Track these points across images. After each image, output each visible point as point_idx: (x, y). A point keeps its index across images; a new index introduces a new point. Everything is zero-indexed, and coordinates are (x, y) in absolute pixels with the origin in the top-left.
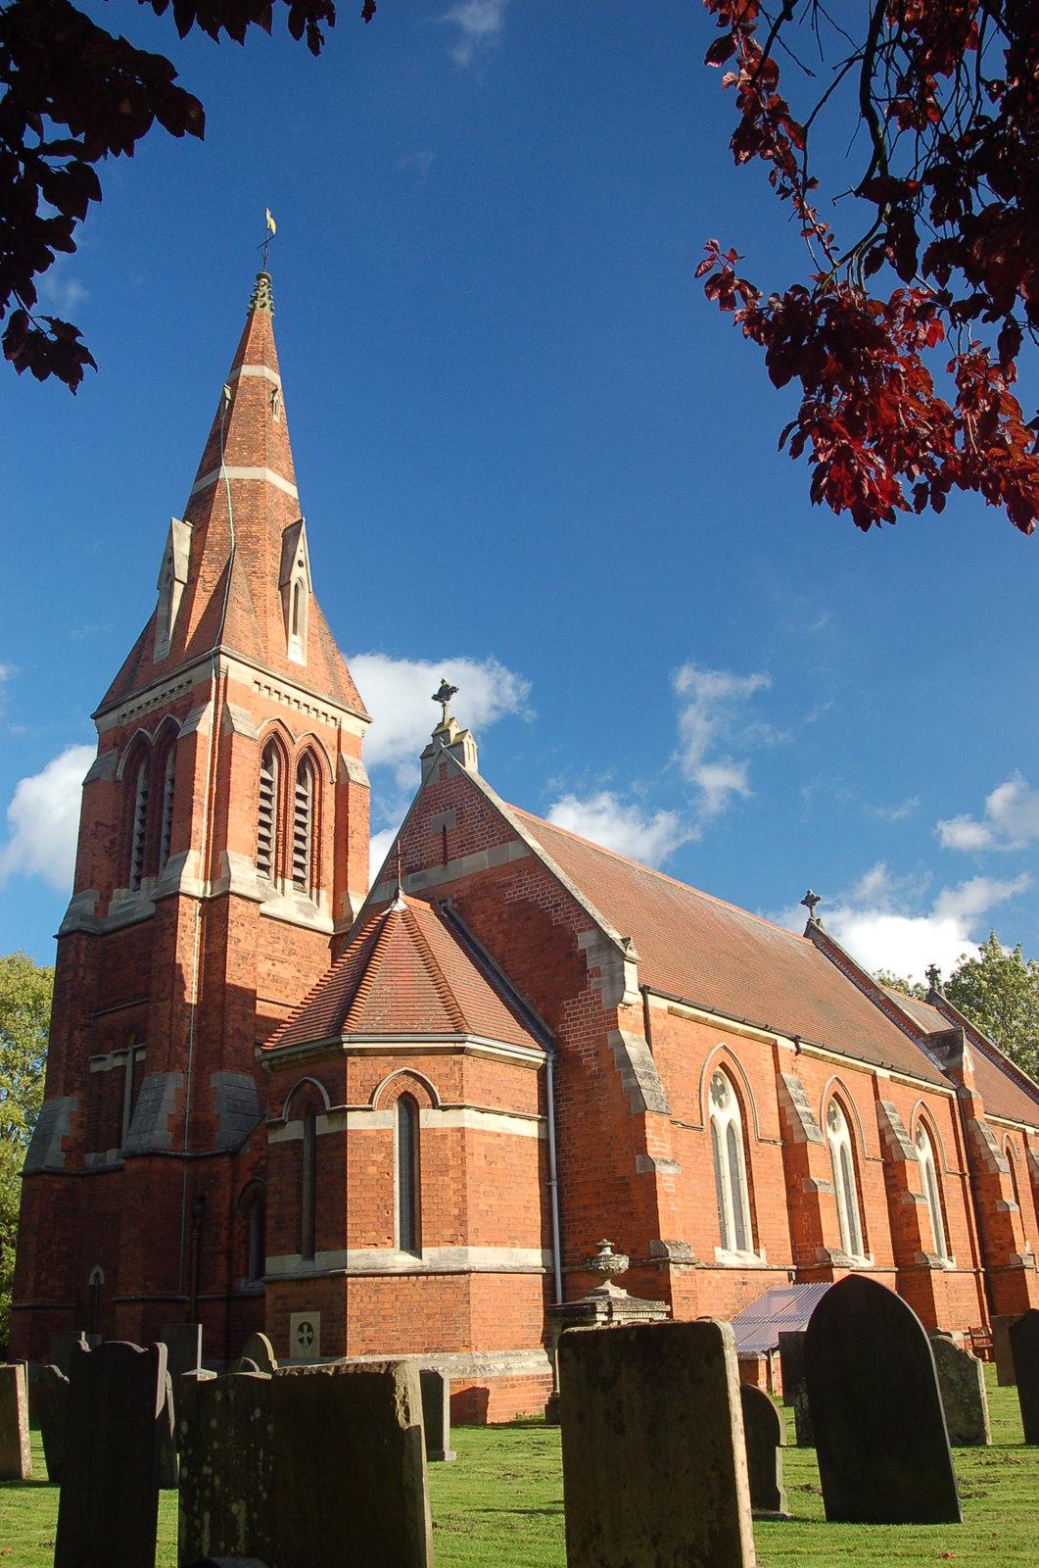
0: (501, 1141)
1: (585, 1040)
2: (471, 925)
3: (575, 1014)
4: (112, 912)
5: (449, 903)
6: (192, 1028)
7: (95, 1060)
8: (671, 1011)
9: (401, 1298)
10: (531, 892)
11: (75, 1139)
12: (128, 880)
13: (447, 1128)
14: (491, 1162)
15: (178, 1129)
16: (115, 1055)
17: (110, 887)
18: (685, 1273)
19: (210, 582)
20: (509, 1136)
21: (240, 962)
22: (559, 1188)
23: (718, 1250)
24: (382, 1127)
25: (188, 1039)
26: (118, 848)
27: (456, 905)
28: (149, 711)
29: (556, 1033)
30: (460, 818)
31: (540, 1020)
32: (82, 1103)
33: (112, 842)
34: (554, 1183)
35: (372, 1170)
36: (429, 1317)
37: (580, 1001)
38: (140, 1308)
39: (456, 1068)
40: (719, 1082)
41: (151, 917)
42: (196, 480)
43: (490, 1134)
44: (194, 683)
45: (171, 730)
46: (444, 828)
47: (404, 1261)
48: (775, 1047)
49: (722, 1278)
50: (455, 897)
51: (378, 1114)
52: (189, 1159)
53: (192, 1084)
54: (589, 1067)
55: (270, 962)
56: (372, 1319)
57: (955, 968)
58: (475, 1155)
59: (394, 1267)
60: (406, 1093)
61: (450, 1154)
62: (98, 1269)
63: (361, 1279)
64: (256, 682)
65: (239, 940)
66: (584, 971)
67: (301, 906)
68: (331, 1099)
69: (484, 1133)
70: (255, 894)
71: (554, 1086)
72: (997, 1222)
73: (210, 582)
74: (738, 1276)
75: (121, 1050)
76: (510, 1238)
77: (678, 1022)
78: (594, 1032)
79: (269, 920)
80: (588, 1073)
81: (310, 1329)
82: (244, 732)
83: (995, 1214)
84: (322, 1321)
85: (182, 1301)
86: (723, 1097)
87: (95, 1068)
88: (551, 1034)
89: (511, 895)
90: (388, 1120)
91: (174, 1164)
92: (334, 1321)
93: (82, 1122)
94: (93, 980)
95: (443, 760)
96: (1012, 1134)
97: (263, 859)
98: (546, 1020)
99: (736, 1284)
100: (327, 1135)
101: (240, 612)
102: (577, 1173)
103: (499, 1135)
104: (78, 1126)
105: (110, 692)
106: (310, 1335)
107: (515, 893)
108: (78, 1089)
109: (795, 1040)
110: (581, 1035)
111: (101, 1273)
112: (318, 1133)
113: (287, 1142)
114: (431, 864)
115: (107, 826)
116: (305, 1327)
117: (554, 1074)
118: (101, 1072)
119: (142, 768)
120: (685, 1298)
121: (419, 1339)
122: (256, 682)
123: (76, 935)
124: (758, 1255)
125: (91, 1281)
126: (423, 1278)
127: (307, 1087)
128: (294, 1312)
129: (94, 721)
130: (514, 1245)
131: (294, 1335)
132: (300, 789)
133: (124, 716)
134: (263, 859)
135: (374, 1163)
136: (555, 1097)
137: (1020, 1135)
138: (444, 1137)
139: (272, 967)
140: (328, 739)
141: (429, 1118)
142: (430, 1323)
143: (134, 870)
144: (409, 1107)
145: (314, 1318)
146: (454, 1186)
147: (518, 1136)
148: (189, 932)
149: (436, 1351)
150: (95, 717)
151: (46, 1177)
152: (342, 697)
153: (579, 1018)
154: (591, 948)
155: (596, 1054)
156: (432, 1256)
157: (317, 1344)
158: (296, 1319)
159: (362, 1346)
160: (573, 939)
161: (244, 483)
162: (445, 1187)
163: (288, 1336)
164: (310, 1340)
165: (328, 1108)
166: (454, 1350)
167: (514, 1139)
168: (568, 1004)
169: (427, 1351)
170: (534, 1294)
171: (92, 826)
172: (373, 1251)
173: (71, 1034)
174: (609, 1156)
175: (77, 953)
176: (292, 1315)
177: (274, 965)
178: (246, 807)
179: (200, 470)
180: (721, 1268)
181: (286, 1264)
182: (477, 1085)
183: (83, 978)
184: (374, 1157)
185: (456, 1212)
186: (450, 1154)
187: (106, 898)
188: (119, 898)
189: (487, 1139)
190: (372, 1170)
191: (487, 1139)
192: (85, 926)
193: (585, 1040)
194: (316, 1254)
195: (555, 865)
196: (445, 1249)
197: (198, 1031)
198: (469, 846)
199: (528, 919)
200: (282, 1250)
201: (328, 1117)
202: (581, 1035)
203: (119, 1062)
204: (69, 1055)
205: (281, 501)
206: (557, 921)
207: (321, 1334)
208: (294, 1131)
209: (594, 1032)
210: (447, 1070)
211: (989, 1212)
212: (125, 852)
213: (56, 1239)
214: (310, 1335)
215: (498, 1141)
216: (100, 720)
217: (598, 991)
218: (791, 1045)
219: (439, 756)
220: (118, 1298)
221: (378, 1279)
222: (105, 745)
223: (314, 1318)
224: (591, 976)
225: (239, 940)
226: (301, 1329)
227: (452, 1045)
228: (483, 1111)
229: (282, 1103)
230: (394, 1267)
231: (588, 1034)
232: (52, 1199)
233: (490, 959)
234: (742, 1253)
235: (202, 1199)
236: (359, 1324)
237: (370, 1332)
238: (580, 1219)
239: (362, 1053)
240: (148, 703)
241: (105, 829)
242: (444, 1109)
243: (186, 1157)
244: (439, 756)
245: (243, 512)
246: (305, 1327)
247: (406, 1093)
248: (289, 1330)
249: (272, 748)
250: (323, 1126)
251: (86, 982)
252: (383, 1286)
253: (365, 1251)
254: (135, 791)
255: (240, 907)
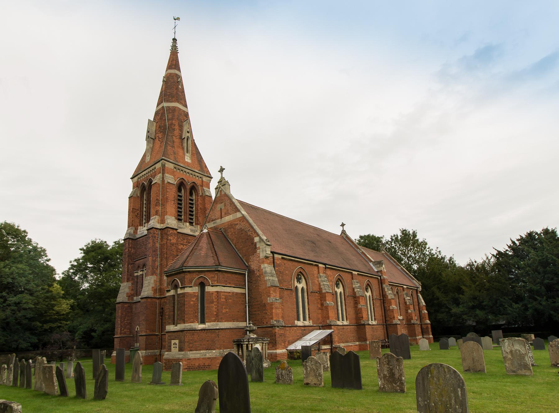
0: (230, 294)
1: (256, 267)
2: (228, 235)
3: (253, 259)
4: (138, 233)
5: (222, 229)
6: (158, 264)
7: (135, 272)
8: (282, 258)
9: (200, 336)
10: (243, 226)
11: (131, 293)
12: (142, 224)
13: (213, 291)
14: (227, 300)
15: (155, 291)
16: (140, 271)
17: (138, 226)
18: (281, 329)
19: (161, 138)
20: (233, 293)
21: (171, 246)
22: (248, 306)
23: (296, 322)
24: (195, 291)
25: (157, 266)
26: (139, 215)
27: (224, 230)
28: (145, 176)
29: (249, 265)
30: (225, 206)
31: (245, 261)
32: (132, 284)
33: (138, 214)
34: (247, 305)
35: (192, 303)
36: (208, 341)
37: (255, 256)
38: (145, 337)
39: (216, 275)
40: (299, 277)
41: (146, 235)
42: (157, 107)
43: (226, 292)
44: (156, 168)
45: (151, 181)
46: (221, 208)
47: (201, 326)
48: (317, 266)
49: (297, 329)
50: (224, 228)
51: (194, 288)
52: (159, 298)
53: (159, 278)
54: (257, 274)
55: (182, 246)
56: (192, 342)
57: (67, 267)
58: (222, 298)
59: (198, 328)
60: (202, 282)
61: (214, 298)
62: (138, 327)
63: (189, 332)
64: (175, 168)
65: (171, 240)
66: (256, 248)
67: (191, 230)
68: (181, 284)
69: (225, 292)
70: (176, 227)
71: (248, 279)
72: (390, 312)
73: (161, 138)
74: (303, 328)
75: (142, 270)
76: (233, 319)
77: (285, 262)
78: (258, 264)
79: (182, 234)
80: (256, 275)
81: (176, 344)
82: (171, 182)
83: (389, 310)
84: (179, 342)
85: (158, 335)
86: (301, 281)
87: (136, 274)
88: (247, 265)
89: (238, 227)
90: (196, 290)
91: (154, 300)
92: (181, 342)
93: (132, 289)
94: (134, 251)
95: (220, 189)
96: (399, 288)
97: (180, 218)
98: (246, 261)
99: (301, 330)
100: (180, 294)
101: (169, 147)
102: (253, 302)
103: (230, 293)
104: (132, 290)
105: (135, 171)
106: (176, 346)
107: (239, 226)
108: (131, 280)
109: (325, 264)
110: (255, 265)
111: (138, 328)
112: (178, 293)
113: (171, 295)
114: (218, 219)
115: (136, 209)
116: (175, 344)
117: (248, 276)
118: (137, 276)
119: (145, 193)
120: (280, 335)
121: (205, 347)
122: (175, 168)
123: (128, 239)
124: (310, 322)
125: (136, 330)
126: (206, 331)
127: (176, 281)
128: (172, 340)
129: (131, 180)
130: (234, 322)
131: (172, 346)
132: (190, 198)
133: (139, 178)
134: (180, 218)
135: (193, 301)
136: (248, 282)
137: (401, 288)
138: (212, 294)
139: (183, 247)
140: (198, 181)
141: (208, 289)
142: (208, 342)
143: (144, 221)
144: (202, 285)
145: (177, 341)
146: (215, 307)
147: (236, 293)
148: (156, 238)
149: (209, 350)
150: (132, 178)
151: (122, 304)
152: (203, 171)
153: (254, 261)
154: (258, 242)
155: (258, 270)
156: (207, 326)
157: (178, 348)
158: (173, 342)
159: (189, 349)
160: (253, 239)
161: (170, 107)
162: (212, 307)
163: (171, 346)
164: (176, 347)
165: (180, 286)
166: (214, 349)
167: (235, 293)
168: (252, 257)
169: (207, 350)
170: (240, 334)
171: (131, 209)
172: (192, 324)
173: (128, 266)
174: (261, 298)
175: (129, 244)
176: (172, 341)
177: (183, 246)
178: (172, 203)
179: (158, 103)
180: (297, 326)
181: (171, 328)
182: (223, 279)
183: (131, 251)
184: (192, 299)
185: (215, 313)
186: (214, 298)
187: (136, 229)
188: (140, 229)
189: (226, 294)
190: (192, 303)
191: (226, 294)
192: (131, 237)
193: (256, 267)
194: (178, 325)
195: (250, 219)
196: (212, 323)
197: (160, 265)
198: (227, 214)
199: (242, 234)
200: (169, 324)
201: (181, 289)
202: (255, 265)
203: (141, 273)
204: (128, 271)
205: (182, 113)
206: (249, 234)
207: (179, 346)
208: (172, 293)
209: (258, 264)
210: (213, 276)
211: (388, 309)
212: (141, 216)
213: (126, 319)
214: (176, 346)
215: (229, 294)
216: (133, 179)
217: (259, 253)
218: (324, 266)
219: (219, 188)
220: (139, 335)
221: (193, 331)
222: (135, 186)
223: (177, 341)
224: (258, 249)
225: (171, 240)
226: (174, 344)
227: (215, 269)
228: (224, 286)
229: (169, 285)
230: (198, 328)
231: (256, 265)
232: (124, 309)
233: (233, 245)
234: (304, 322)
235: (162, 308)
236: (188, 343)
237: (191, 345)
238: (254, 314)
239: (189, 272)
240: (145, 174)
241: (135, 210)
242: (212, 286)
243: (157, 298)
244: (219, 188)
245: (170, 117)
246: (175, 344)
247: (202, 282)
248: (171, 344)
249: (181, 185)
250: (180, 291)
251: (132, 252)
252: (194, 333)
253: (190, 324)
254: (143, 200)
255: (171, 231)
